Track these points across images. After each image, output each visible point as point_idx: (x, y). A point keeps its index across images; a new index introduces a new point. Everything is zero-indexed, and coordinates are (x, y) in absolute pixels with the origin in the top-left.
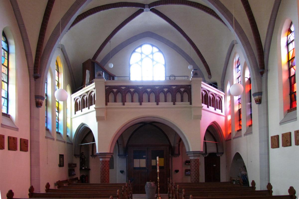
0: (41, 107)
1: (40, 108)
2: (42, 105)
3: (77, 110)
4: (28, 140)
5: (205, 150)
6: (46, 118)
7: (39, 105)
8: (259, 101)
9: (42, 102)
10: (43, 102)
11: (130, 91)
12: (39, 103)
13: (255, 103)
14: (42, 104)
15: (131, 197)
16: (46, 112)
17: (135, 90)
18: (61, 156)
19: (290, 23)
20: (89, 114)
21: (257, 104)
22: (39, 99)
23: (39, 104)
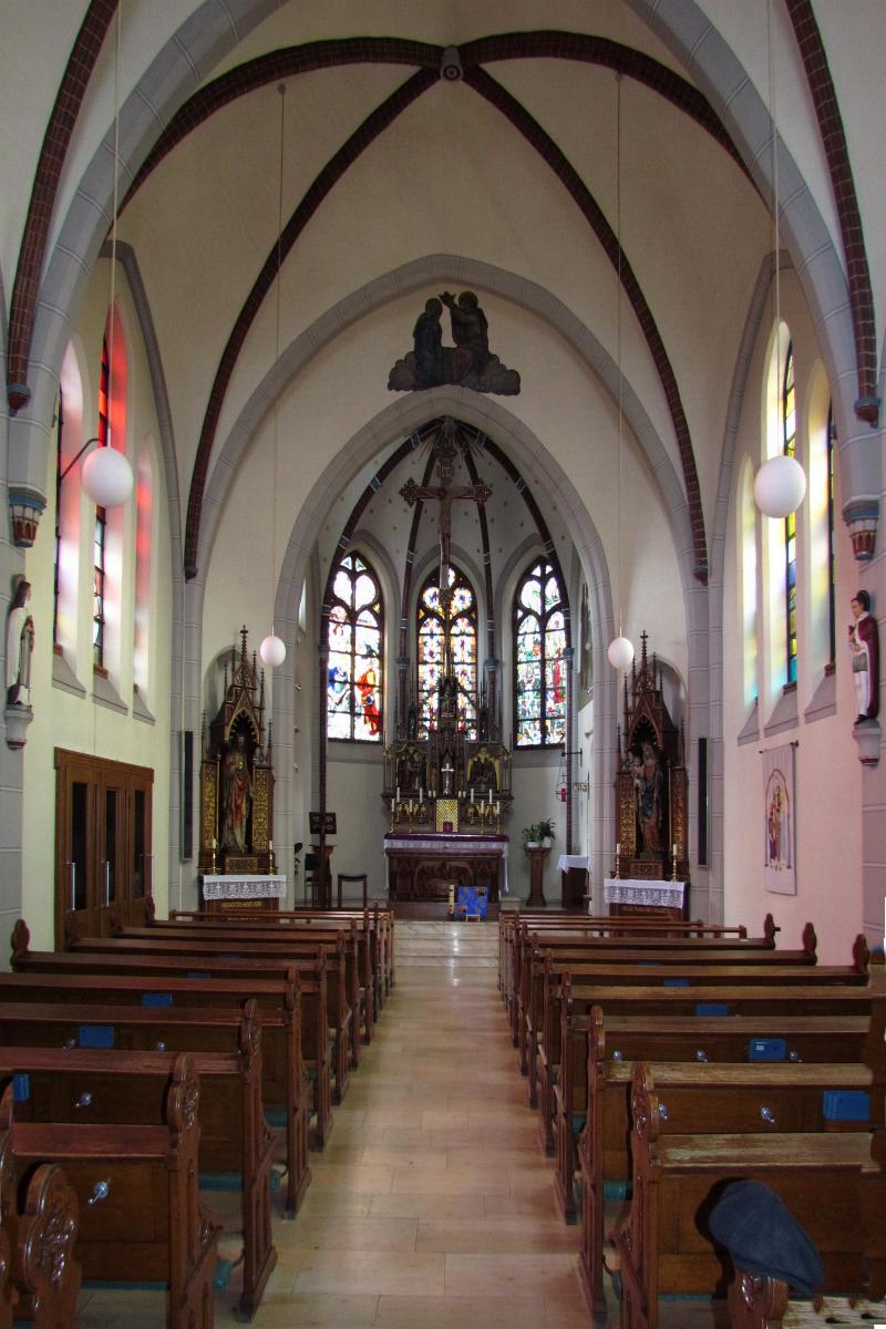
0: (30, 546)
1: (27, 549)
2: (33, 538)
3: (460, 427)
4: (148, 774)
5: (830, 973)
6: (96, 626)
7: (23, 536)
8: (867, 544)
9: (33, 521)
10: (37, 523)
11: (413, 64)
12: (24, 527)
13: (853, 556)
14: (35, 529)
15: (777, 1316)
16: (835, 582)
17: (421, 72)
18: (375, 1021)
19: (133, 626)
20: (55, 551)
21: (859, 558)
22: (25, 507)
23: (24, 532)
